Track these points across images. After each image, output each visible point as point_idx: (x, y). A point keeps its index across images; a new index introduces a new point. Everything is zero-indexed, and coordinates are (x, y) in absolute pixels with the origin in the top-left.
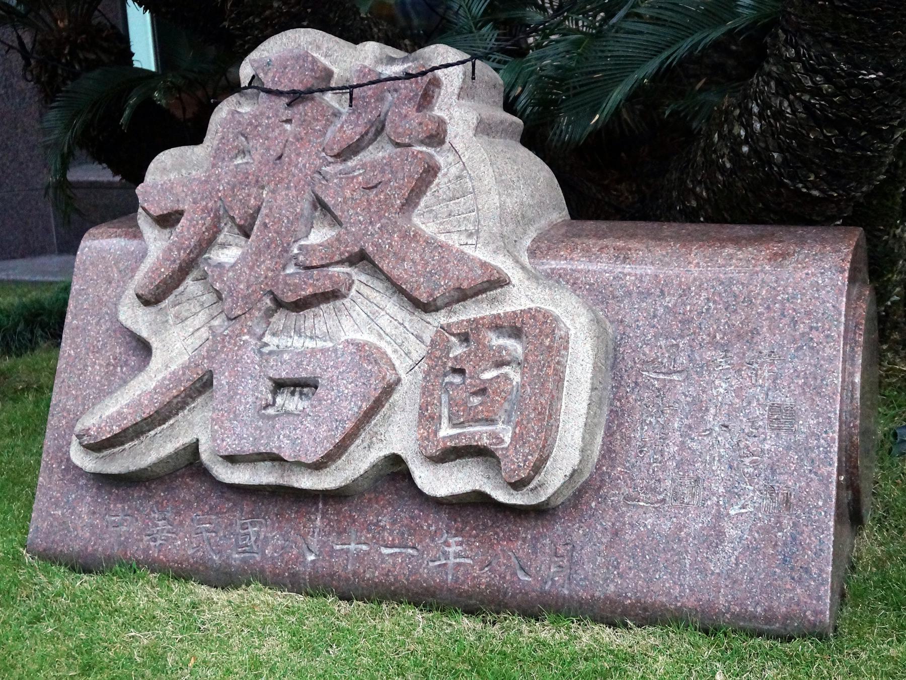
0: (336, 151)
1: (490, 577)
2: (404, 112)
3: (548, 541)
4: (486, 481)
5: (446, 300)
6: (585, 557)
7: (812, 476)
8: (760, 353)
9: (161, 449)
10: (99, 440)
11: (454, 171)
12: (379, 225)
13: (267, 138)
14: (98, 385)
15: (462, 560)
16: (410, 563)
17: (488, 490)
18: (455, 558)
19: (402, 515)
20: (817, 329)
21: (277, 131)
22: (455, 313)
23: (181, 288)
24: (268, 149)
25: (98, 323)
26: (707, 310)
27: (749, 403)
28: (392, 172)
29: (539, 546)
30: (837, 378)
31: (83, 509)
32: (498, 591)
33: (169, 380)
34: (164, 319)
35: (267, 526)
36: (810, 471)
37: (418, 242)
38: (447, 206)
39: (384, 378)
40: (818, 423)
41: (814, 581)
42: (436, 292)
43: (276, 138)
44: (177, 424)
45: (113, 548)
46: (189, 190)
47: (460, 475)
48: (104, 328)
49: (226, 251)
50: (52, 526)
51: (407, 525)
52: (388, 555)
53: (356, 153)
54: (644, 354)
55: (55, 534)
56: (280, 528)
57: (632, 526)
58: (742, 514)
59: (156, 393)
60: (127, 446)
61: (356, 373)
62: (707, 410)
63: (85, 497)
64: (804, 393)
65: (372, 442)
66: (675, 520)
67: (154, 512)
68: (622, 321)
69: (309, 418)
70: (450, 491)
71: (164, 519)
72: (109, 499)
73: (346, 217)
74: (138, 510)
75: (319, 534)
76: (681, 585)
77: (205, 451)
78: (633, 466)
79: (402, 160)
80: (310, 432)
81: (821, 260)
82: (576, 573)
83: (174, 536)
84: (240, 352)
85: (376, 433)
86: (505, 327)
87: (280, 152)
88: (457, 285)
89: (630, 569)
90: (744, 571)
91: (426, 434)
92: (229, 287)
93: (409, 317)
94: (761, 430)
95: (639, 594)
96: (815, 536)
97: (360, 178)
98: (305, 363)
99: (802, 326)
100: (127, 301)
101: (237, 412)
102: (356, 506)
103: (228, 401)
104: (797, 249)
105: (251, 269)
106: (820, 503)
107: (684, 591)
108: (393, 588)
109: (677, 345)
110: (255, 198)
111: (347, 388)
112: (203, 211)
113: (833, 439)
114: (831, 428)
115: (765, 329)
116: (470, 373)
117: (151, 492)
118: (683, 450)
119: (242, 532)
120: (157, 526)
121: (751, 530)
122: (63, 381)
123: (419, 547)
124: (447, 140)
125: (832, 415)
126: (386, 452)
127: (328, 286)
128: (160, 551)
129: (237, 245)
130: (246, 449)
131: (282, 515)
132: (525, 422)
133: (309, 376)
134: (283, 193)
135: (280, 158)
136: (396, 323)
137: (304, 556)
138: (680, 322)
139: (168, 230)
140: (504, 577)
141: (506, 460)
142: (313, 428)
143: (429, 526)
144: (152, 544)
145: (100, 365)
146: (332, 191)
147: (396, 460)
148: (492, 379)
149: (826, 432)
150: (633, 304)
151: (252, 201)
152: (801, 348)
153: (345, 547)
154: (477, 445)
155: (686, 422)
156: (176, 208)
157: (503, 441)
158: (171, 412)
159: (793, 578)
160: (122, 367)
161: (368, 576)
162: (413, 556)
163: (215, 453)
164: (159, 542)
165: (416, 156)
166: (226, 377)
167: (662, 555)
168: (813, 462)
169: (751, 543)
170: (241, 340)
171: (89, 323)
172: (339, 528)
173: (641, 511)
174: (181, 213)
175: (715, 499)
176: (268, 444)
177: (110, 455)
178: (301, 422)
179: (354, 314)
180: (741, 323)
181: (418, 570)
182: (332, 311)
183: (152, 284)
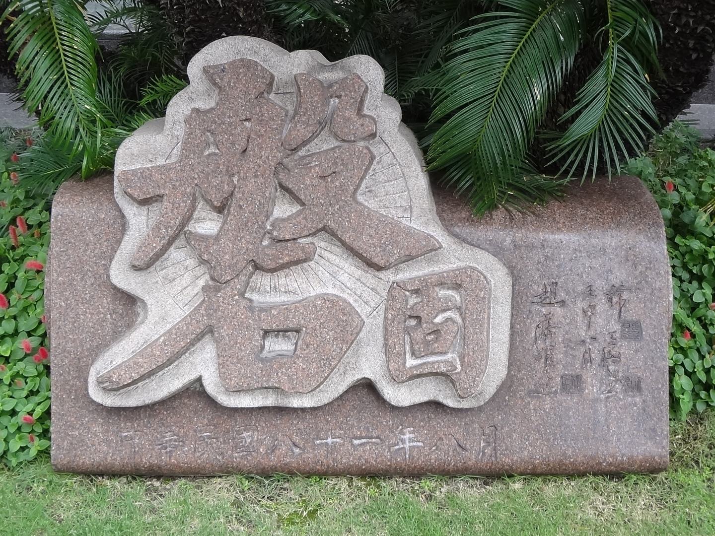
7: (654, 368)
9: (171, 385)
15: (415, 444)
17: (441, 399)
18: (409, 442)
21: (239, 129)
24: (233, 144)
25: (82, 279)
29: (471, 429)
35: (258, 431)
37: (372, 220)
41: (659, 437)
47: (418, 390)
48: (89, 283)
49: (201, 224)
50: (72, 444)
52: (358, 445)
70: (412, 401)
79: (350, 155)
84: (234, 310)
87: (244, 146)
88: (407, 253)
91: (396, 366)
95: (544, 456)
97: (317, 169)
99: (640, 267)
101: (240, 357)
102: (328, 411)
106: (660, 386)
107: (575, 452)
111: (328, 335)
120: (164, 437)
122: (59, 328)
126: (358, 377)
129: (210, 219)
132: (471, 353)
134: (253, 180)
135: (245, 151)
136: (354, 279)
139: (146, 207)
145: (92, 314)
153: (324, 441)
157: (456, 368)
161: (344, 461)
162: (378, 444)
164: (168, 449)
169: (617, 416)
172: (316, 428)
182: (301, 272)
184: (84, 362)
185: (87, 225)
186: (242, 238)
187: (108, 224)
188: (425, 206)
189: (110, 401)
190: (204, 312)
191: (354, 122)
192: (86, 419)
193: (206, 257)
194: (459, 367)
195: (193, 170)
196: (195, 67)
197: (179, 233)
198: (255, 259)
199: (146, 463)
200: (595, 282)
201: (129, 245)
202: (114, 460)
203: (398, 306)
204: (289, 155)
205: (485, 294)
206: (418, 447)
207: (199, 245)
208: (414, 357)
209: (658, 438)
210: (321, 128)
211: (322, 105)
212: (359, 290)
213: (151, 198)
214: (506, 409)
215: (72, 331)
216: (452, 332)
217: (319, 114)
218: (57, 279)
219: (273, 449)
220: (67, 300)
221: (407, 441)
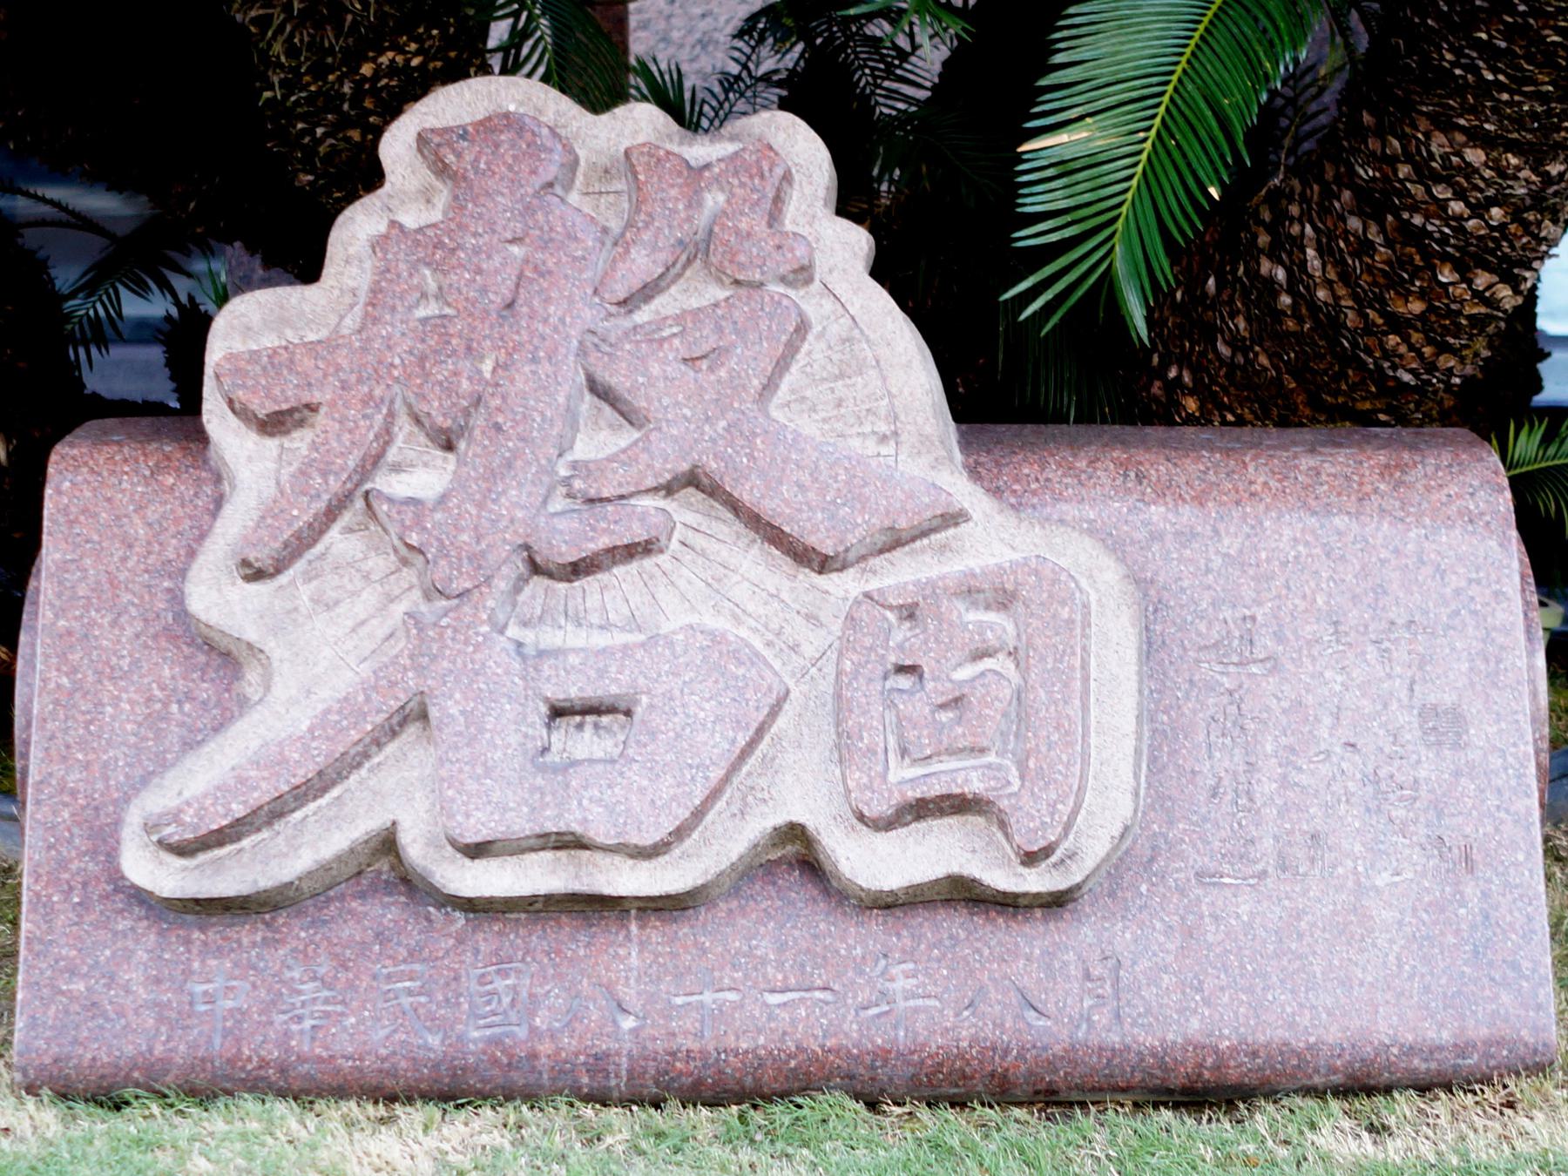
0: (622, 296)
1: (975, 1026)
2: (743, 226)
3: (1071, 956)
4: (969, 856)
5: (863, 551)
6: (1141, 977)
7: (1502, 815)
8: (1393, 623)
9: (321, 844)
10: (203, 831)
11: (840, 327)
12: (723, 423)
13: (479, 271)
14: (132, 739)
15: (920, 1002)
16: (824, 1015)
18: (906, 999)
19: (797, 933)
20: (1478, 582)
22: (875, 573)
23: (319, 548)
25: (114, 623)
26: (1295, 557)
27: (1385, 706)
28: (737, 332)
30: (1520, 657)
31: (132, 975)
32: (994, 1049)
33: (339, 712)
34: (289, 606)
36: (1498, 807)
38: (832, 390)
39: (770, 689)
40: (1500, 731)
42: (850, 536)
43: (497, 272)
44: (348, 795)
45: (210, 1041)
46: (329, 364)
48: (129, 631)
50: (67, 1012)
51: (808, 951)
52: (779, 1006)
53: (648, 299)
54: (1199, 634)
55: (77, 1027)
56: (560, 976)
57: (1216, 918)
58: (1396, 884)
59: (314, 738)
60: (246, 843)
61: (716, 682)
62: (1317, 720)
63: (133, 952)
64: (1472, 684)
65: (746, 804)
66: (1286, 902)
67: (289, 968)
68: (1152, 582)
69: (635, 767)
71: (314, 979)
72: (189, 951)
73: (657, 410)
74: (255, 968)
75: (638, 980)
76: (1313, 1007)
77: (414, 841)
78: (1205, 820)
80: (642, 790)
81: (1461, 472)
82: (1129, 1004)
83: (339, 1008)
84: (478, 656)
85: (752, 788)
86: (984, 591)
87: (509, 296)
88: (887, 523)
89: (1222, 989)
90: (1411, 977)
91: (865, 780)
92: (439, 540)
93: (786, 584)
94: (1410, 747)
95: (1242, 1030)
96: (1519, 909)
97: (676, 342)
98: (613, 669)
99: (1454, 577)
100: (205, 574)
101: (490, 763)
102: (704, 925)
103: (468, 745)
104: (1417, 458)
105: (480, 506)
106: (1521, 857)
108: (793, 1063)
109: (1253, 618)
110: (470, 379)
112: (365, 403)
113: (1526, 754)
114: (1522, 736)
115: (1395, 586)
116: (932, 672)
117: (278, 931)
118: (1285, 788)
119: (482, 989)
121: (1414, 910)
123: (836, 987)
124: (817, 277)
125: (1520, 717)
126: (780, 819)
127: (638, 533)
128: (313, 1039)
130: (516, 828)
131: (558, 952)
133: (624, 690)
137: (614, 1022)
138: (1253, 579)
140: (1003, 1025)
141: (1019, 814)
142: (645, 783)
143: (849, 948)
144: (294, 1027)
145: (131, 702)
146: (624, 365)
147: (794, 833)
148: (973, 679)
149: (1515, 745)
150: (1168, 552)
151: (465, 384)
152: (1457, 613)
154: (963, 794)
155: (1284, 740)
156: (306, 397)
158: (339, 774)
159: (1492, 979)
160: (179, 702)
162: (827, 1003)
163: (431, 843)
165: (779, 303)
166: (457, 702)
167: (1274, 963)
168: (1499, 791)
170: (477, 634)
171: (93, 623)
173: (1228, 893)
174: (312, 408)
175: (1350, 863)
176: (560, 816)
177: (213, 862)
178: (621, 774)
179: (682, 583)
180: (1356, 577)
181: (840, 1026)
182: (637, 579)
183: (276, 538)
184: (108, 815)
185: (132, 501)
186: (499, 494)
187: (182, 498)
188: (928, 430)
189: (168, 878)
190: (408, 662)
191: (760, 240)
192: (108, 952)
193: (414, 539)
194: (1016, 784)
195: (389, 348)
196: (397, 145)
197: (353, 498)
198: (530, 541)
199: (249, 1059)
200: (1345, 615)
201: (234, 526)
202: (171, 1050)
203: (868, 641)
204: (611, 315)
205: (1072, 611)
206: (926, 1009)
207: (399, 513)
208: (907, 760)
209: (1525, 984)
210: (684, 257)
211: (689, 206)
212: (775, 620)
213: (291, 411)
214: (1145, 915)
215: (83, 744)
216: (997, 698)
217: (680, 226)
218: (54, 624)
219: (574, 1017)
220: (74, 670)
221: (899, 998)
